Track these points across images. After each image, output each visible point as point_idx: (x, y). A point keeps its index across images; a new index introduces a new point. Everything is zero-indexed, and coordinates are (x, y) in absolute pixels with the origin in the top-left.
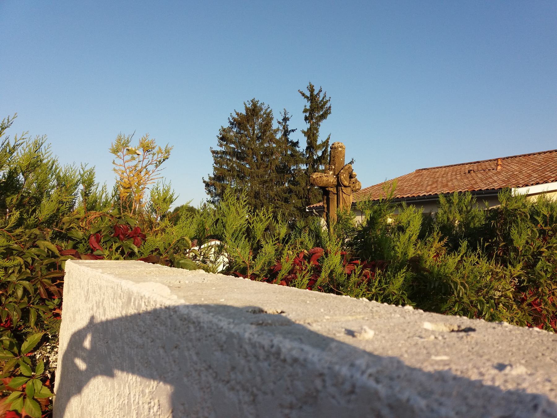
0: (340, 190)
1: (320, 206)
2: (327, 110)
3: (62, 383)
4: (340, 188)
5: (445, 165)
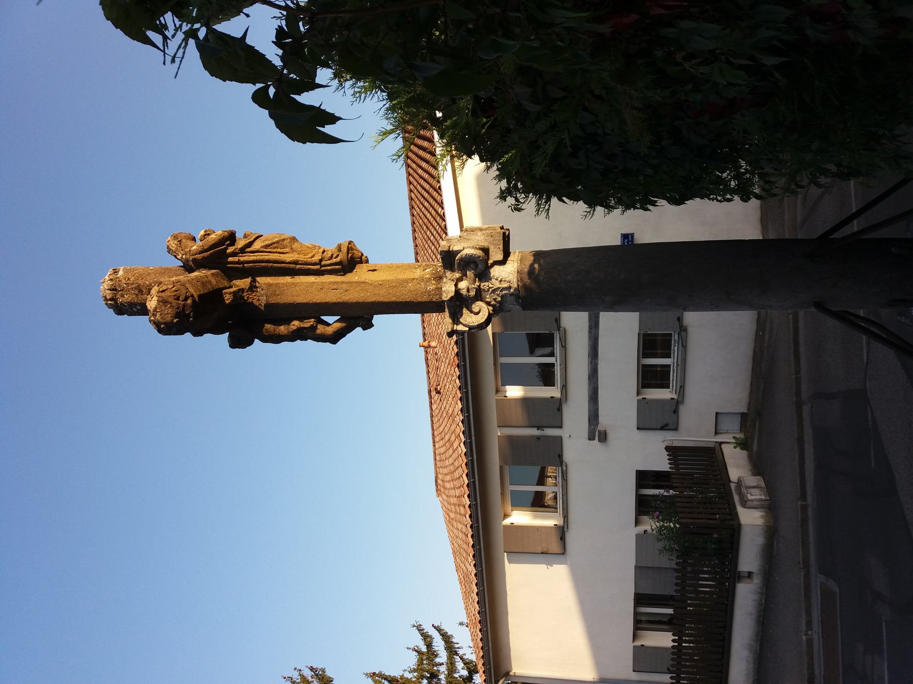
0: (239, 262)
1: (483, 664)
2: (317, 675)
3: (557, 322)
4: (230, 259)
5: (432, 446)
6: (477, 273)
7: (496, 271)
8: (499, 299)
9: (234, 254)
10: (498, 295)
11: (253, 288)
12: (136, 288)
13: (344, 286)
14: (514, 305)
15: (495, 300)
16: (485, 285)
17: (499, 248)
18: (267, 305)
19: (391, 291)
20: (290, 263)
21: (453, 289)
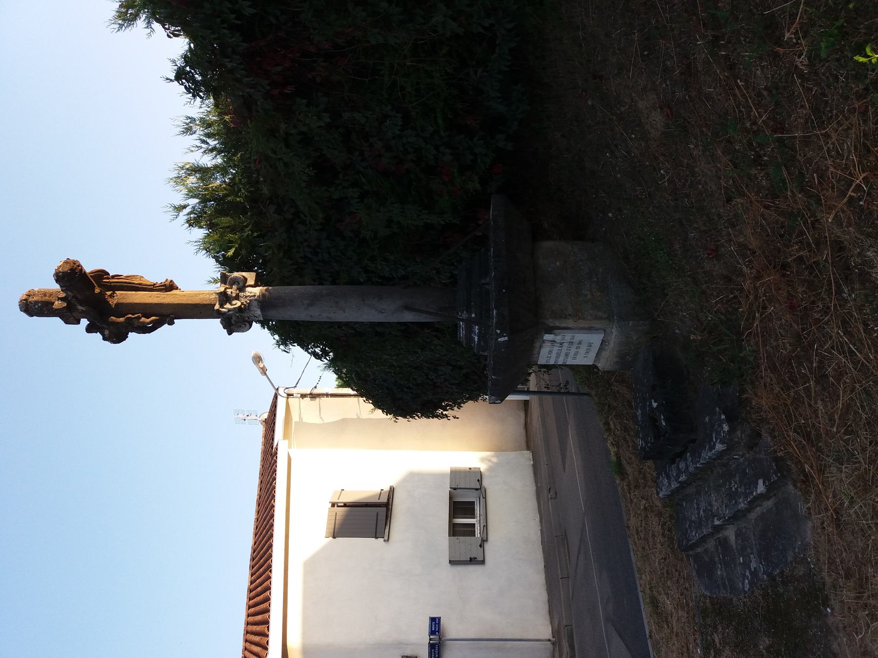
0: (108, 282)
4: (104, 280)
7: (249, 289)
9: (108, 278)
10: (248, 300)
11: (111, 296)
12: (43, 294)
13: (164, 296)
15: (246, 302)
16: (241, 294)
18: (117, 305)
19: (189, 299)
20: (137, 284)
21: (224, 289)
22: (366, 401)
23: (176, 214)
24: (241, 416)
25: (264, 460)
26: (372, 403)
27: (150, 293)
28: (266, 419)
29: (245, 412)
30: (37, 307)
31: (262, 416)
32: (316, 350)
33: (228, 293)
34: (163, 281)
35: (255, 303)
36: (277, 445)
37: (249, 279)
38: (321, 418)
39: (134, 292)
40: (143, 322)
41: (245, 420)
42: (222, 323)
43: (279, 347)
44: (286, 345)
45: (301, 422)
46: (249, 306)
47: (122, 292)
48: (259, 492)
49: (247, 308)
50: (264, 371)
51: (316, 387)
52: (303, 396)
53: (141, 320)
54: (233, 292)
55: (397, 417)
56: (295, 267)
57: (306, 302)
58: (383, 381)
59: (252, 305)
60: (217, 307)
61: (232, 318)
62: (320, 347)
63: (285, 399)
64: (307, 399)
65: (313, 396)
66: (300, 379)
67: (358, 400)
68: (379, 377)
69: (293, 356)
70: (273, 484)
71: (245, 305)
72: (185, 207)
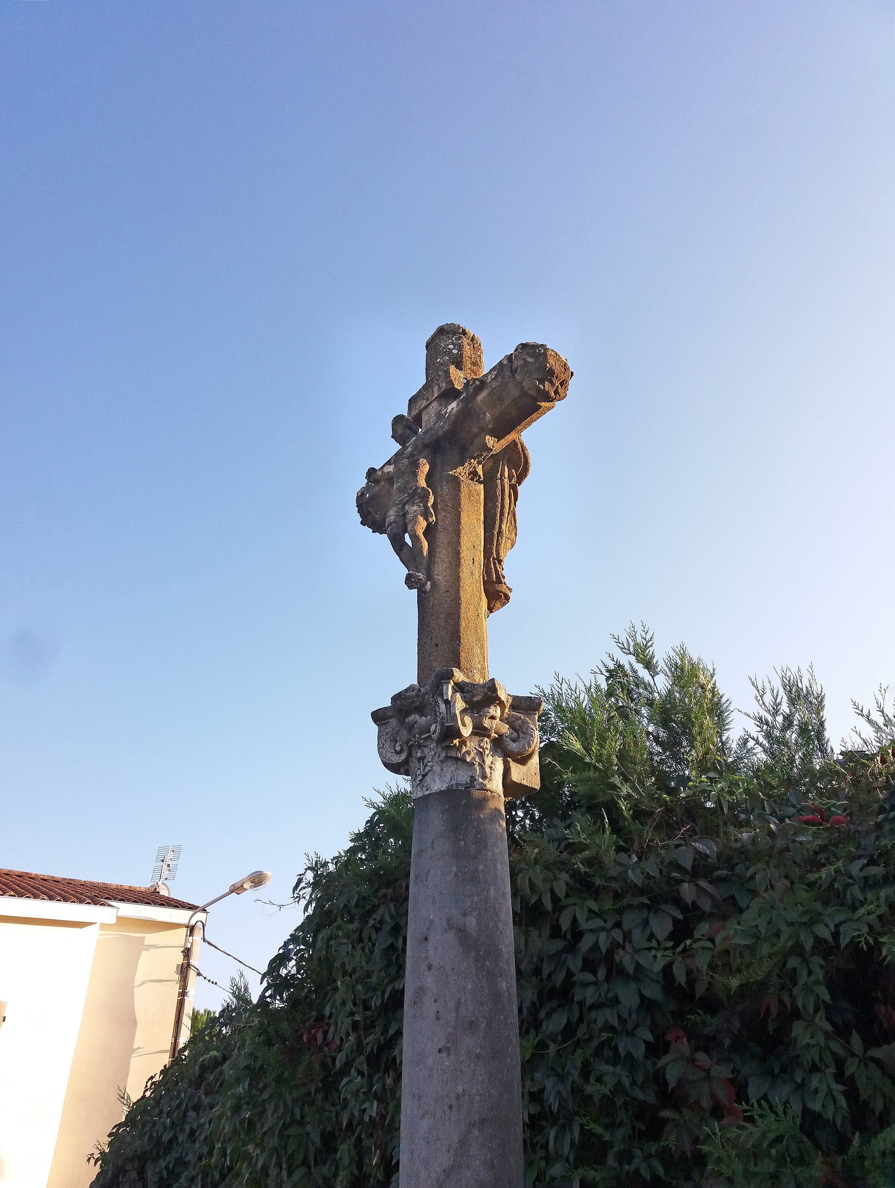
0: (502, 475)
6: (504, 738)
8: (468, 759)
14: (451, 779)
15: (468, 753)
16: (487, 743)
17: (524, 779)
18: (456, 482)
20: (500, 527)
22: (150, 1082)
23: (632, 649)
24: (170, 855)
25: (93, 886)
26: (144, 1097)
27: (482, 548)
28: (158, 892)
29: (174, 863)
30: (451, 347)
31: (164, 887)
32: (293, 963)
33: (492, 707)
34: (508, 581)
35: (463, 777)
36: (109, 905)
37: (523, 769)
38: (143, 983)
39: (482, 518)
40: (415, 521)
41: (163, 861)
42: (411, 688)
43: (309, 868)
44: (315, 885)
45: (141, 946)
46: (457, 759)
47: (482, 497)
48: (42, 877)
49: (452, 754)
50: (237, 889)
51: (199, 974)
52: (187, 953)
53: (421, 519)
54: (494, 722)
55: (100, 1162)
56: (548, 904)
57: (472, 922)
58: (191, 1129)
59: (457, 769)
60: (459, 676)
61: (422, 715)
62: (298, 972)
63: (186, 922)
64: (180, 959)
65: (184, 970)
66: (216, 948)
67: (165, 1051)
68: (202, 1121)
69: (281, 906)
70: (42, 896)
71: (459, 749)
72: (649, 665)
